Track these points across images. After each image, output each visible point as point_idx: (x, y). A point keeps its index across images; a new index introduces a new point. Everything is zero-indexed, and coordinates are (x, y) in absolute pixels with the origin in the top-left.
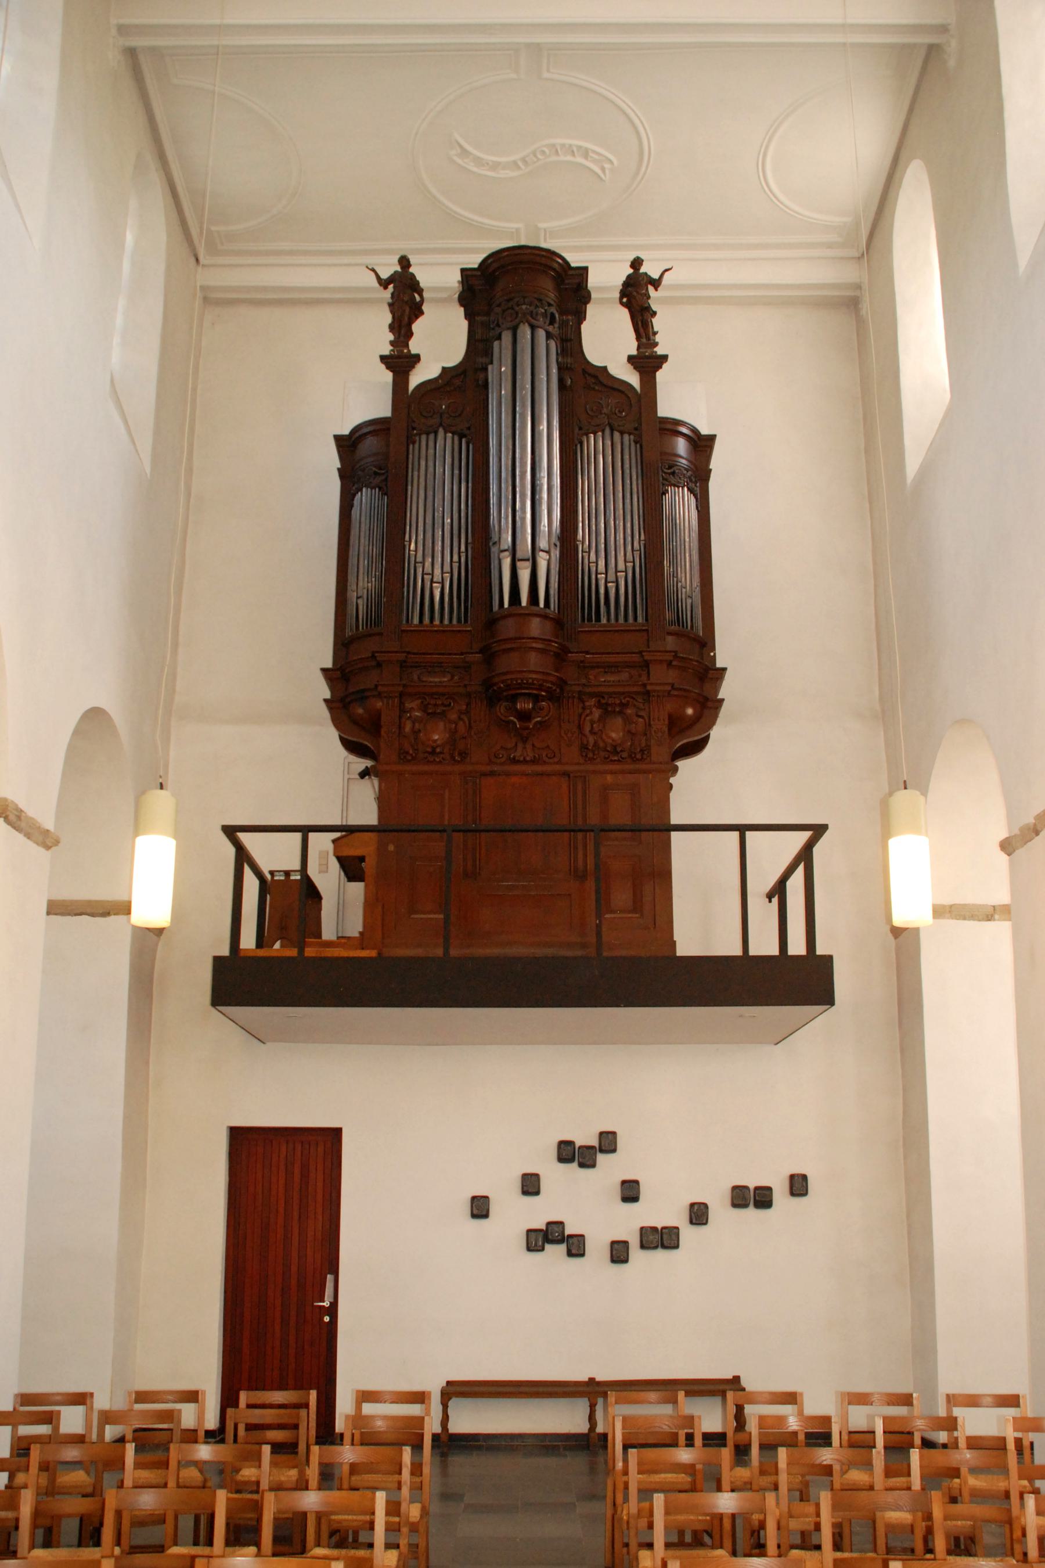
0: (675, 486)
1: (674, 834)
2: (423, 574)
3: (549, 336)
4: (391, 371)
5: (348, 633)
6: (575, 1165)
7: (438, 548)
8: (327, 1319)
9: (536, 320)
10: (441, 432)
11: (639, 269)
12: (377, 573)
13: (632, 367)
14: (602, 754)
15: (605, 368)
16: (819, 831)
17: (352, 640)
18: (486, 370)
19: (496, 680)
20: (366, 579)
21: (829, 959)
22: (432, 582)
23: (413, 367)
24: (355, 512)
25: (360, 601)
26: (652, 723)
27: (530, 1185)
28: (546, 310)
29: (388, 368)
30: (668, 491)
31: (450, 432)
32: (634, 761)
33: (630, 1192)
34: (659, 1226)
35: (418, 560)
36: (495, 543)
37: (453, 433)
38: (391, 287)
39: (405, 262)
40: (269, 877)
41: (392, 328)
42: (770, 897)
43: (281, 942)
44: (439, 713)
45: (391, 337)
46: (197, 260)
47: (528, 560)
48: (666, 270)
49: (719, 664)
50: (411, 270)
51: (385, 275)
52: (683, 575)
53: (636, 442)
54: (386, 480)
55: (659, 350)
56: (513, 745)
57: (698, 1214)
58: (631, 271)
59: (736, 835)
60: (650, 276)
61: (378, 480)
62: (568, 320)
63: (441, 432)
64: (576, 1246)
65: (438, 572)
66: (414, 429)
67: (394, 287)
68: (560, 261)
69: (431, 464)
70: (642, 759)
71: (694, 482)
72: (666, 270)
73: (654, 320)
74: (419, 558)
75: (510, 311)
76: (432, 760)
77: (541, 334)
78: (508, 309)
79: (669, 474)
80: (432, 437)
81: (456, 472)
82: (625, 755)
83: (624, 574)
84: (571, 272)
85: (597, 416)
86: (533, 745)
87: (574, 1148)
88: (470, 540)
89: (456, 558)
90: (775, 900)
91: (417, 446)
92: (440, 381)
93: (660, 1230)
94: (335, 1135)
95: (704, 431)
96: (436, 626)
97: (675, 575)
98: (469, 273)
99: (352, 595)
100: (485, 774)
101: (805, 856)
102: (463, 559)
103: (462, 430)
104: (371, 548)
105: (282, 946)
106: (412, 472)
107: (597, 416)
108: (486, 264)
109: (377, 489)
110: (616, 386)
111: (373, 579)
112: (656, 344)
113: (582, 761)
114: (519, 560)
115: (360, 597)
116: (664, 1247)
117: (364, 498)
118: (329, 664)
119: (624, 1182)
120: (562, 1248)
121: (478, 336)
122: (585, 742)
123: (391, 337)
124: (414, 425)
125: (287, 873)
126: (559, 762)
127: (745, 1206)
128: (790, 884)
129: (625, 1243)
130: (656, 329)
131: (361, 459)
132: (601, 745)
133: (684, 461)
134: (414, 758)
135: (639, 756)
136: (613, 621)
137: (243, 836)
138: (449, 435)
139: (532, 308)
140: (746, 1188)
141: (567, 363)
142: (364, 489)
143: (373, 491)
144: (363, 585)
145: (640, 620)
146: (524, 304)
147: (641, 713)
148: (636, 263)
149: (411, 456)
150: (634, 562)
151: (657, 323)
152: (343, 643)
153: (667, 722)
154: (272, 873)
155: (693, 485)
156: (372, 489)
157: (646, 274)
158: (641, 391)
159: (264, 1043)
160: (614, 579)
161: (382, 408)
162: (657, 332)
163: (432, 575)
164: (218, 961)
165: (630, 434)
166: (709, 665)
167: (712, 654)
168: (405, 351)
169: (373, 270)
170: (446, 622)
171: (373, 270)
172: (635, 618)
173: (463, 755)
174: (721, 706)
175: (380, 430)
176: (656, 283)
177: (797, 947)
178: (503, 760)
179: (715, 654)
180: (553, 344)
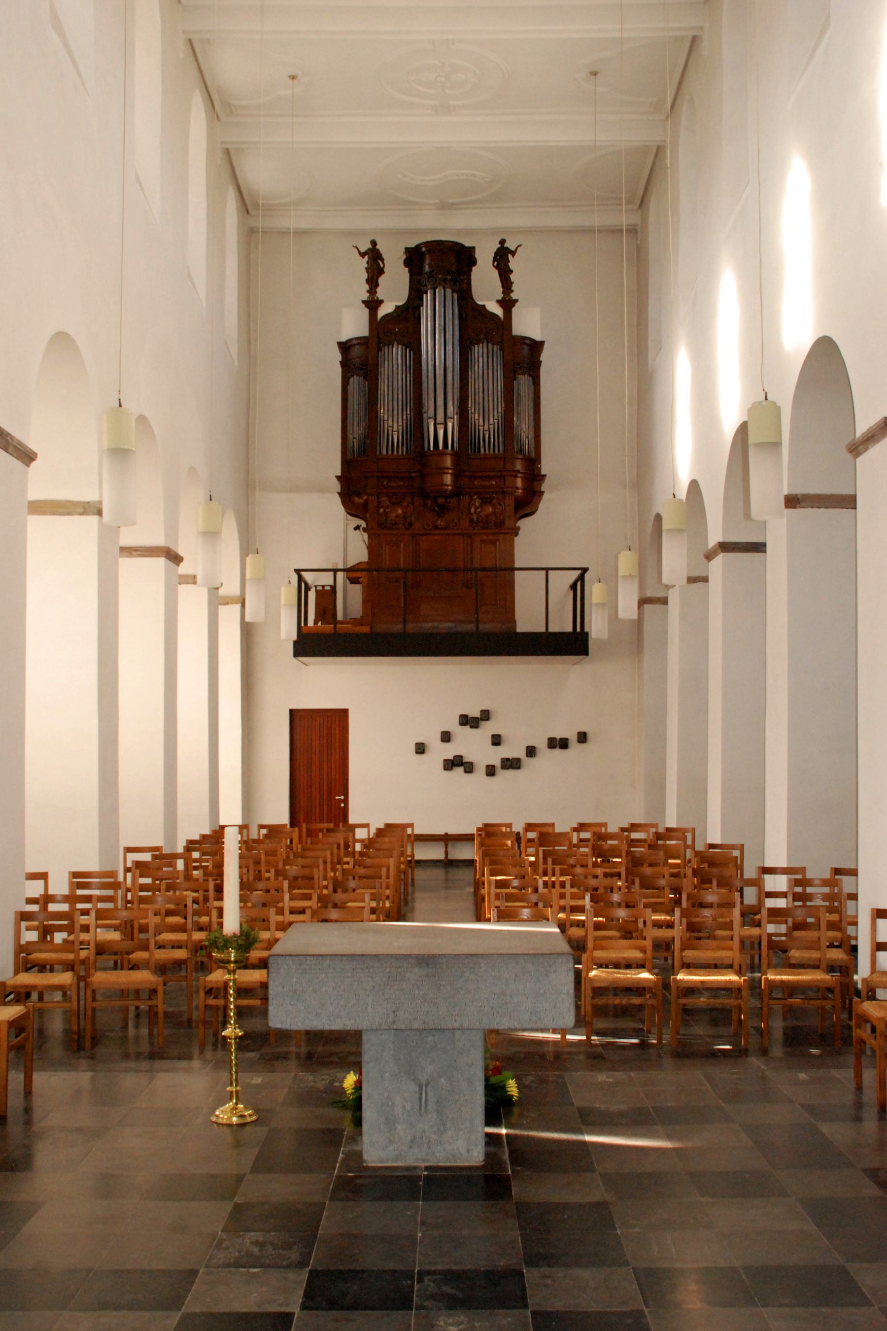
2: (388, 427)
5: (349, 457)
6: (468, 727)
8: (342, 805)
10: (395, 344)
15: (484, 306)
16: (585, 570)
22: (393, 431)
23: (380, 306)
27: (446, 737)
33: (497, 740)
34: (510, 757)
36: (425, 412)
37: (402, 345)
38: (366, 257)
41: (368, 281)
45: (366, 266)
46: (248, 212)
48: (519, 246)
49: (543, 473)
51: (362, 250)
57: (531, 752)
58: (499, 246)
59: (544, 572)
63: (395, 344)
64: (469, 768)
65: (395, 425)
66: (381, 343)
67: (369, 258)
72: (519, 246)
74: (386, 418)
75: (433, 278)
77: (449, 291)
80: (391, 346)
86: (446, 520)
87: (467, 719)
89: (405, 418)
91: (383, 353)
94: (346, 711)
99: (350, 436)
100: (420, 535)
102: (409, 418)
105: (321, 624)
112: (512, 291)
114: (438, 424)
117: (355, 381)
118: (339, 474)
119: (493, 736)
120: (461, 769)
123: (366, 266)
124: (382, 341)
125: (323, 587)
129: (493, 766)
130: (512, 281)
131: (351, 359)
136: (487, 452)
138: (400, 347)
140: (555, 739)
142: (355, 376)
144: (357, 431)
148: (502, 242)
151: (513, 277)
152: (347, 463)
157: (507, 248)
158: (504, 316)
159: (307, 665)
163: (393, 427)
169: (356, 248)
171: (356, 248)
176: (513, 253)
178: (431, 528)
180: (456, 296)
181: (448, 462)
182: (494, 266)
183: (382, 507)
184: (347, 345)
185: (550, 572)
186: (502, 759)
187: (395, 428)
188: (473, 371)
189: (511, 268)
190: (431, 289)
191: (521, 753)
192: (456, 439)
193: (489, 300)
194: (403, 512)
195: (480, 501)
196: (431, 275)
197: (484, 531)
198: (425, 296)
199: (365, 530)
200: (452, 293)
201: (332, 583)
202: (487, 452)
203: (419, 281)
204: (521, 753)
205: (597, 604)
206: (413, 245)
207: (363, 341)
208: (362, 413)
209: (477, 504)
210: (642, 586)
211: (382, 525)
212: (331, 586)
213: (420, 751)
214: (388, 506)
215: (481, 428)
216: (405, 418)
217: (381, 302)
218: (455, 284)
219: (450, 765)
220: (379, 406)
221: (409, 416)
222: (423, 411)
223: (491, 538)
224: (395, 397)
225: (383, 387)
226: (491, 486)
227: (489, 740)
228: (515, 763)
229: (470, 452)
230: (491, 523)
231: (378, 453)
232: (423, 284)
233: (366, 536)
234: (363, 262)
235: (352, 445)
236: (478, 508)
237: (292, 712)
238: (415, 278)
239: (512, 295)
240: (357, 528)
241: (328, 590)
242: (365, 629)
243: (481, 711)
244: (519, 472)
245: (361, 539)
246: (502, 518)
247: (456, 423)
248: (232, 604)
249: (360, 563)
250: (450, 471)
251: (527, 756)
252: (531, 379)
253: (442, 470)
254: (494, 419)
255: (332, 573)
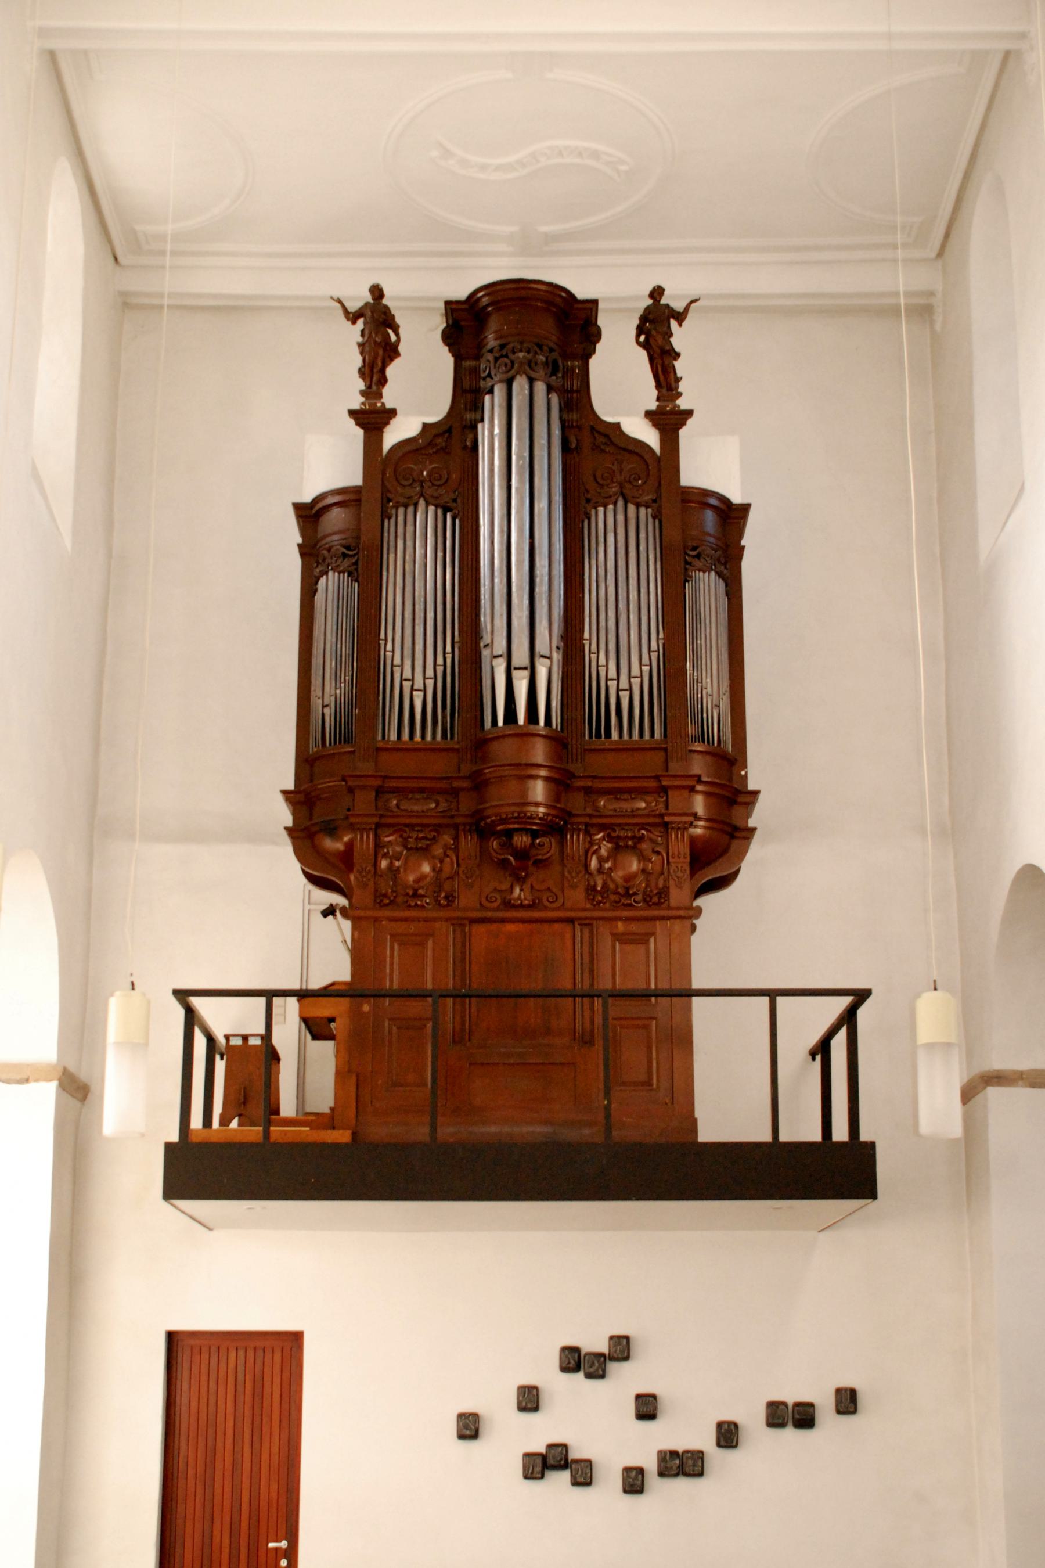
0: (699, 570)
1: (695, 999)
3: (550, 389)
4: (362, 428)
5: (313, 749)
6: (581, 1375)
7: (419, 647)
9: (534, 370)
10: (422, 503)
11: (659, 301)
12: (347, 678)
13: (651, 424)
14: (613, 897)
15: (618, 425)
16: (861, 996)
17: (318, 758)
18: (475, 428)
19: (489, 812)
20: (334, 685)
21: (872, 1146)
22: (412, 689)
24: (319, 598)
25: (327, 711)
26: (671, 860)
28: (547, 358)
29: (358, 424)
30: (691, 577)
31: (433, 505)
32: (650, 906)
35: (395, 663)
36: (486, 646)
37: (436, 506)
38: (360, 323)
39: (377, 292)
40: (222, 1041)
41: (362, 372)
42: (813, 1054)
43: (239, 1120)
44: (421, 848)
45: (360, 340)
47: (525, 668)
50: (385, 301)
51: (353, 306)
52: (709, 680)
53: (654, 517)
54: (356, 563)
55: (683, 403)
56: (509, 886)
58: (650, 302)
60: (672, 309)
61: (347, 563)
62: (573, 369)
63: (422, 503)
66: (389, 500)
67: (365, 324)
68: (563, 294)
69: (409, 543)
70: (658, 904)
71: (722, 564)
73: (676, 363)
74: (397, 661)
75: (506, 360)
76: (413, 904)
77: (540, 387)
78: (502, 356)
79: (694, 557)
80: (411, 509)
81: (440, 554)
82: (639, 898)
83: (639, 679)
84: (576, 306)
85: (607, 485)
86: (532, 887)
87: (579, 1357)
88: (457, 639)
89: (440, 661)
90: (818, 1058)
91: (393, 521)
92: (420, 441)
93: (681, 1454)
94: (295, 1339)
95: (736, 498)
96: (417, 743)
97: (700, 680)
98: (454, 306)
99: (316, 703)
100: (473, 921)
101: (849, 1018)
103: (446, 502)
104: (339, 646)
105: (240, 1125)
106: (388, 554)
107: (607, 485)
108: (475, 298)
109: (346, 575)
110: (631, 448)
111: (343, 685)
112: (680, 395)
113: (588, 906)
114: (515, 669)
115: (327, 706)
116: (687, 1475)
117: (329, 584)
118: (290, 786)
120: (565, 1476)
121: (466, 385)
122: (592, 883)
123: (360, 340)
124: (390, 496)
125: (245, 1038)
126: (562, 907)
127: (782, 1425)
128: (834, 1042)
129: (641, 1471)
130: (679, 375)
131: (325, 537)
132: (612, 886)
133: (712, 540)
134: (392, 902)
135: (655, 899)
136: (626, 736)
137: (196, 1001)
139: (530, 356)
140: (785, 1404)
141: (572, 421)
142: (330, 573)
143: (341, 575)
145: (657, 735)
146: (521, 351)
147: (658, 849)
149: (386, 534)
150: (651, 665)
153: (688, 860)
154: (227, 1037)
155: (723, 567)
156: (339, 573)
157: (667, 306)
158: (661, 448)
160: (627, 686)
161: (352, 475)
162: (681, 378)
163: (413, 680)
164: (169, 1147)
165: (647, 507)
166: (740, 788)
167: (743, 773)
168: (379, 405)
169: (339, 301)
170: (429, 738)
172: (652, 735)
173: (450, 898)
174: (753, 836)
175: (350, 501)
176: (680, 317)
177: (840, 1133)
178: (495, 905)
179: (746, 773)
180: (555, 399)
181: (539, 752)
182: (638, 342)
183: (385, 855)
184: (317, 508)
185: (780, 1000)
186: (660, 1452)
187: (419, 683)
188: (594, 562)
189: (677, 349)
190: (501, 381)
191: (704, 1440)
192: (555, 703)
193: (628, 414)
194: (433, 869)
195: (609, 845)
196: (503, 352)
197: (618, 913)
198: (487, 398)
199: (345, 913)
200: (549, 393)
201: (262, 1031)
202: (626, 736)
203: (475, 372)
204: (704, 1440)
205: (930, 1046)
206: (461, 292)
207: (352, 497)
208: (345, 651)
209: (603, 852)
210: (969, 1056)
211: (380, 900)
212: (262, 1037)
213: (468, 1432)
214: (401, 853)
215: (613, 685)
216: (440, 661)
217: (391, 414)
218: (554, 373)
219: (539, 1469)
220: (382, 636)
221: (449, 657)
222: (482, 645)
223: (634, 927)
224: (419, 614)
225: (393, 596)
226: (634, 813)
227: (630, 1408)
228: (690, 1462)
229: (587, 737)
230: (635, 894)
231: (380, 737)
232: (483, 375)
233: (347, 925)
234: (354, 332)
235: (320, 717)
236: (607, 861)
237: (172, 1337)
238: (467, 364)
239: (678, 402)
240: (329, 911)
241: (255, 1046)
242: (343, 1136)
243: (611, 1338)
244: (698, 779)
245: (340, 939)
246: (661, 884)
247: (555, 669)
248: (37, 1080)
249: (333, 984)
250: (543, 773)
251: (719, 1445)
252: (721, 584)
253: (524, 772)
254: (641, 664)
255: (262, 1001)
